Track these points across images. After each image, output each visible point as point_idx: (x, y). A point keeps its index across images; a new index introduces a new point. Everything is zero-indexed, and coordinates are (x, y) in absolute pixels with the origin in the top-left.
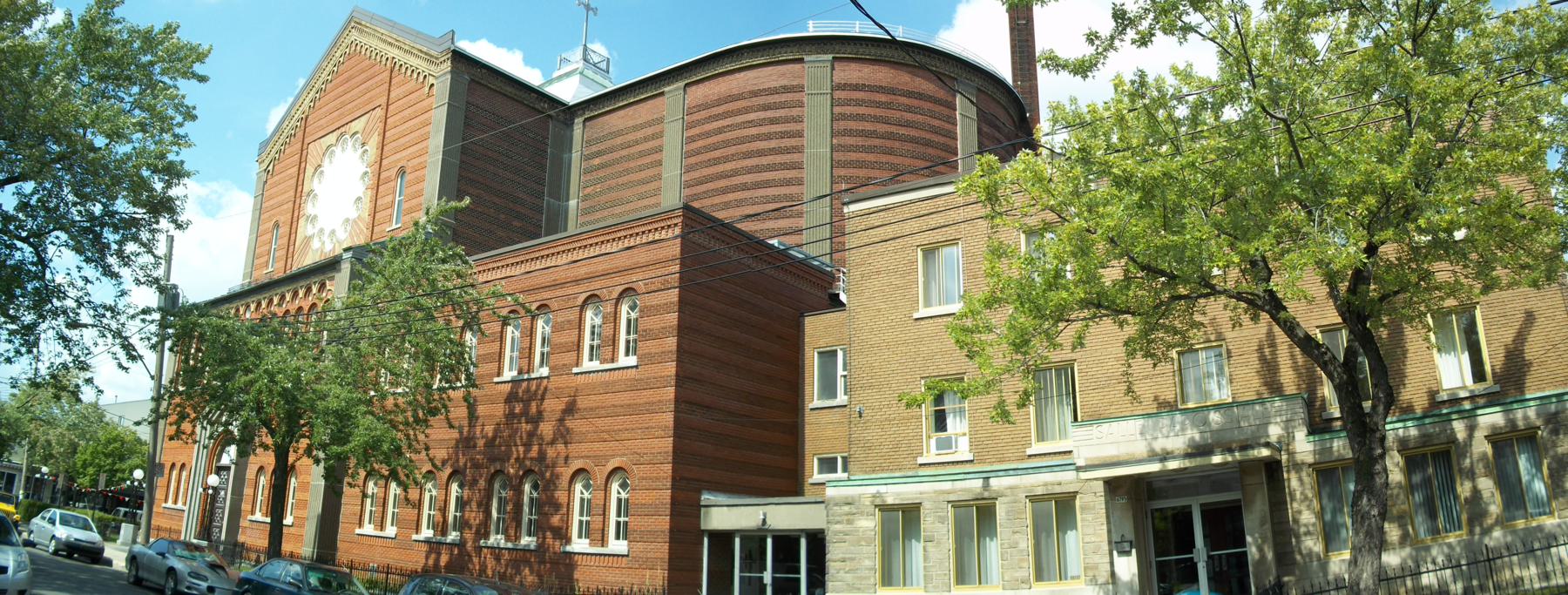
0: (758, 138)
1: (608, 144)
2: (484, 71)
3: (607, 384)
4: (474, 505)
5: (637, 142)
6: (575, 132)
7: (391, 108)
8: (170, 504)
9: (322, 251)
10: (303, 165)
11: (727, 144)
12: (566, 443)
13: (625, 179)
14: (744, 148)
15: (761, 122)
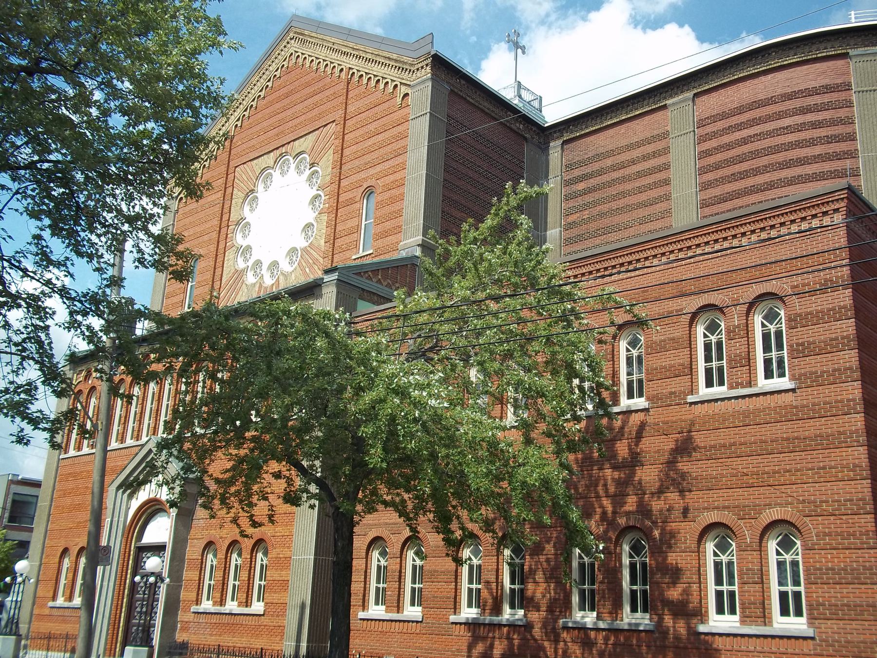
0: (798, 144)
1: (596, 166)
2: (463, 82)
3: (746, 414)
4: (540, 576)
5: (633, 162)
6: (551, 157)
7: (349, 123)
8: (60, 601)
9: (261, 286)
10: (229, 190)
11: (756, 154)
12: (682, 492)
13: (621, 203)
14: (780, 157)
15: (801, 128)
